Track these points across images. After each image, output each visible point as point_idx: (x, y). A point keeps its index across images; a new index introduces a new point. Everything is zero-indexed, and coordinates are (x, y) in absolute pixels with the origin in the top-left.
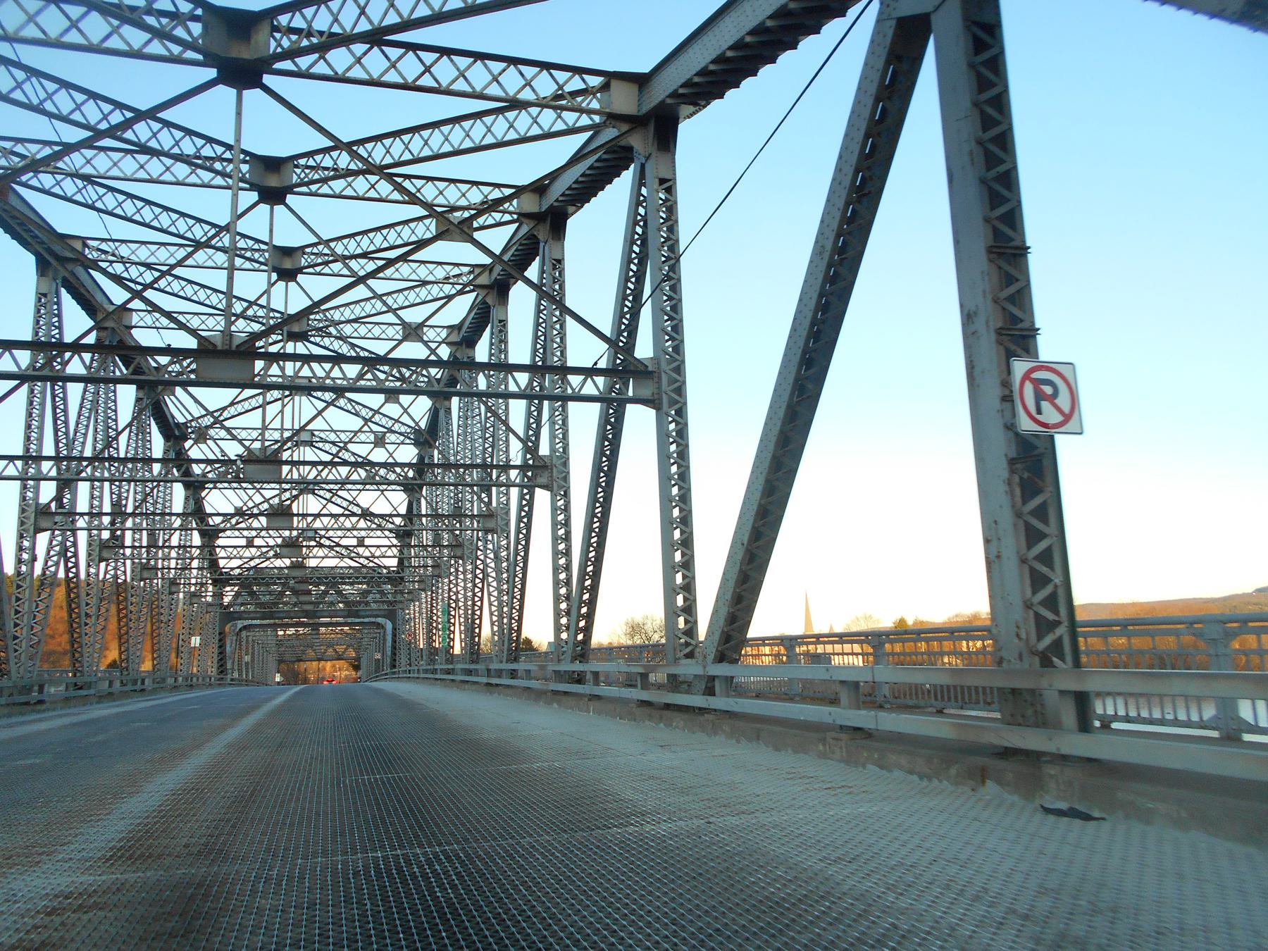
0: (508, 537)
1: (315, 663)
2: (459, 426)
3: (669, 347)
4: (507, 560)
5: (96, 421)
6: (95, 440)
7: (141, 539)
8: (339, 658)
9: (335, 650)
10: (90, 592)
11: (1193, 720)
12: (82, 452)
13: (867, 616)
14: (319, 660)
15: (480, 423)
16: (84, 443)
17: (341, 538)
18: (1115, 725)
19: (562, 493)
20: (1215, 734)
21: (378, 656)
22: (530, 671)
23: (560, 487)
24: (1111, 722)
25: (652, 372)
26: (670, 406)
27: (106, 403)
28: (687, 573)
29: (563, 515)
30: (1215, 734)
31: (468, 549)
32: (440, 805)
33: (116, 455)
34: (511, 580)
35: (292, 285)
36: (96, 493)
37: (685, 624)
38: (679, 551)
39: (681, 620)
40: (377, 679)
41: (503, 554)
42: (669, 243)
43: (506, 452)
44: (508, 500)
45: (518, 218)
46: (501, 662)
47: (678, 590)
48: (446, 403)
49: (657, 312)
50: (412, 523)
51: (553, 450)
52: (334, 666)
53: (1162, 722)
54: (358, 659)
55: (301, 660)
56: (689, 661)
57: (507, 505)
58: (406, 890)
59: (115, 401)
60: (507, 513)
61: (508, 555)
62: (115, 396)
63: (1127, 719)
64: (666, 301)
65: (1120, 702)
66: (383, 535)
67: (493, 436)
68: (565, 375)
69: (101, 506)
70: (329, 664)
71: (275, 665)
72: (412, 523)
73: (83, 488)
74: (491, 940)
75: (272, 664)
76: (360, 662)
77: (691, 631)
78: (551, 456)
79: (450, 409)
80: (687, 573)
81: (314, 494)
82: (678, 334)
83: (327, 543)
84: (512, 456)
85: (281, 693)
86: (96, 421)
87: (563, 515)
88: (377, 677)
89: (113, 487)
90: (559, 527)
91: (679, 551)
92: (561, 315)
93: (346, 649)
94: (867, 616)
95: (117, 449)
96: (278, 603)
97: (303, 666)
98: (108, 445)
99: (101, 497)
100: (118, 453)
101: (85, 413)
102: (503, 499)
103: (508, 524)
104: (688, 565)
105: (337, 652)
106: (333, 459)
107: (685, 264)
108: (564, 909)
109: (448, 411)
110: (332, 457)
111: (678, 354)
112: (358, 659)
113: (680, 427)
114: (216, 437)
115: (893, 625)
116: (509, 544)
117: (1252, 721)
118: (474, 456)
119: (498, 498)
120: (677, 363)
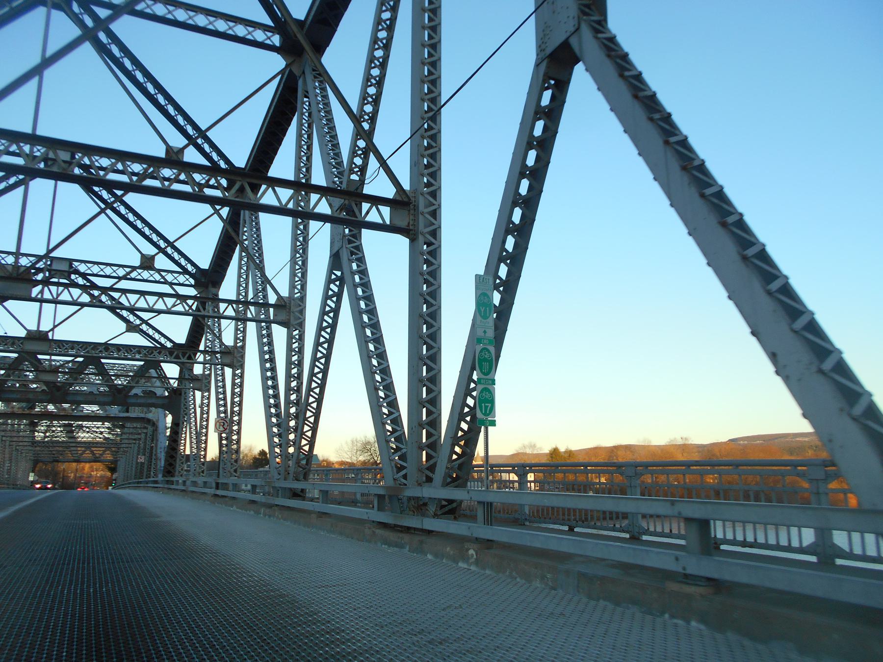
1: (74, 464)
8: (96, 460)
9: (92, 452)
11: (855, 552)
13: (533, 445)
14: (78, 461)
18: (723, 547)
20: (813, 559)
21: (142, 459)
22: (327, 492)
24: (721, 544)
29: (296, 369)
30: (813, 559)
32: (170, 621)
40: (137, 486)
50: (204, 309)
52: (91, 467)
53: (754, 545)
54: (115, 462)
55: (58, 461)
63: (734, 542)
65: (749, 528)
66: (163, 274)
70: (87, 466)
71: (30, 465)
72: (204, 309)
75: (24, 465)
76: (116, 466)
78: (289, 298)
83: (81, 281)
85: (39, 494)
87: (296, 369)
88: (138, 483)
90: (292, 379)
93: (104, 451)
94: (533, 445)
96: (7, 380)
97: (62, 466)
105: (94, 454)
106: (123, 195)
108: (245, 648)
110: (125, 198)
112: (115, 462)
115: (548, 452)
117: (847, 550)
120: (300, 320)
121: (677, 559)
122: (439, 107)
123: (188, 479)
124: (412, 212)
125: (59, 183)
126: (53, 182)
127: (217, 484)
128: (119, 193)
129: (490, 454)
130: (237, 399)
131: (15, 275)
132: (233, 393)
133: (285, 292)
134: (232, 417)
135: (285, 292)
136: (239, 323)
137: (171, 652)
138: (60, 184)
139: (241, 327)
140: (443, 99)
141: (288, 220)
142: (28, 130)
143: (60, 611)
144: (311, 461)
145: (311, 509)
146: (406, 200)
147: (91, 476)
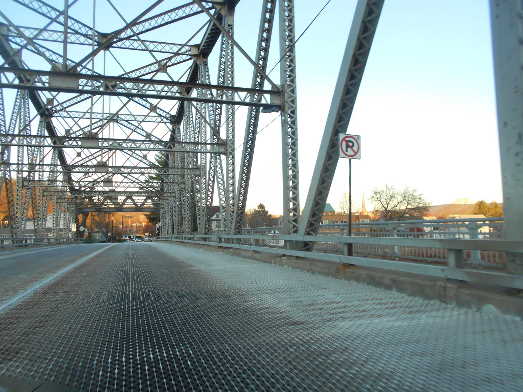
0: (205, 179)
2: (183, 132)
3: (288, 80)
4: (205, 184)
5: (20, 117)
6: (20, 126)
7: (40, 175)
10: (18, 194)
12: (13, 132)
15: (193, 127)
16: (14, 128)
17: (127, 187)
19: (231, 157)
23: (231, 153)
25: (280, 92)
26: (289, 109)
27: (24, 114)
28: (295, 202)
31: (187, 186)
33: (29, 147)
34: (206, 193)
35: (107, 52)
36: (20, 154)
37: (293, 206)
38: (292, 192)
39: (291, 204)
41: (203, 186)
42: (290, 58)
43: (205, 159)
44: (206, 162)
45: (213, 6)
46: (202, 234)
47: (291, 211)
48: (178, 126)
49: (282, 20)
51: (227, 137)
56: (295, 234)
57: (205, 164)
58: (154, 323)
59: (29, 113)
60: (205, 168)
61: (206, 181)
62: (29, 110)
64: (288, 77)
67: (199, 128)
68: (234, 45)
69: (22, 160)
73: (14, 150)
74: (194, 336)
77: (296, 209)
78: (226, 140)
79: (180, 129)
80: (295, 202)
81: (117, 122)
82: (297, 212)
84: (207, 139)
86: (20, 117)
87: (231, 161)
89: (29, 133)
91: (292, 192)
92: (232, 92)
95: (28, 150)
98: (25, 128)
99: (23, 156)
100: (27, 148)
101: (15, 114)
102: (204, 161)
103: (205, 173)
104: (295, 177)
107: (298, 47)
109: (179, 129)
110: (135, 152)
111: (293, 63)
113: (294, 140)
114: (73, 116)
116: (206, 181)
118: (190, 138)
119: (201, 161)
120: (293, 98)
121: (339, 258)
122: (294, 43)
123: (195, 236)
124: (282, 96)
125: (111, 96)
126: (109, 96)
127: (220, 239)
128: (133, 151)
129: (352, 211)
130: (231, 175)
131: (64, 71)
132: (228, 171)
133: (277, 82)
134: (228, 187)
135: (277, 82)
136: (203, 155)
137: (169, 334)
138: (112, 97)
139: (204, 157)
140: (296, 38)
141: (236, 85)
142: (108, 138)
143: (108, 330)
144: (324, 210)
145: (250, 249)
146: (277, 90)
147: (133, 226)
